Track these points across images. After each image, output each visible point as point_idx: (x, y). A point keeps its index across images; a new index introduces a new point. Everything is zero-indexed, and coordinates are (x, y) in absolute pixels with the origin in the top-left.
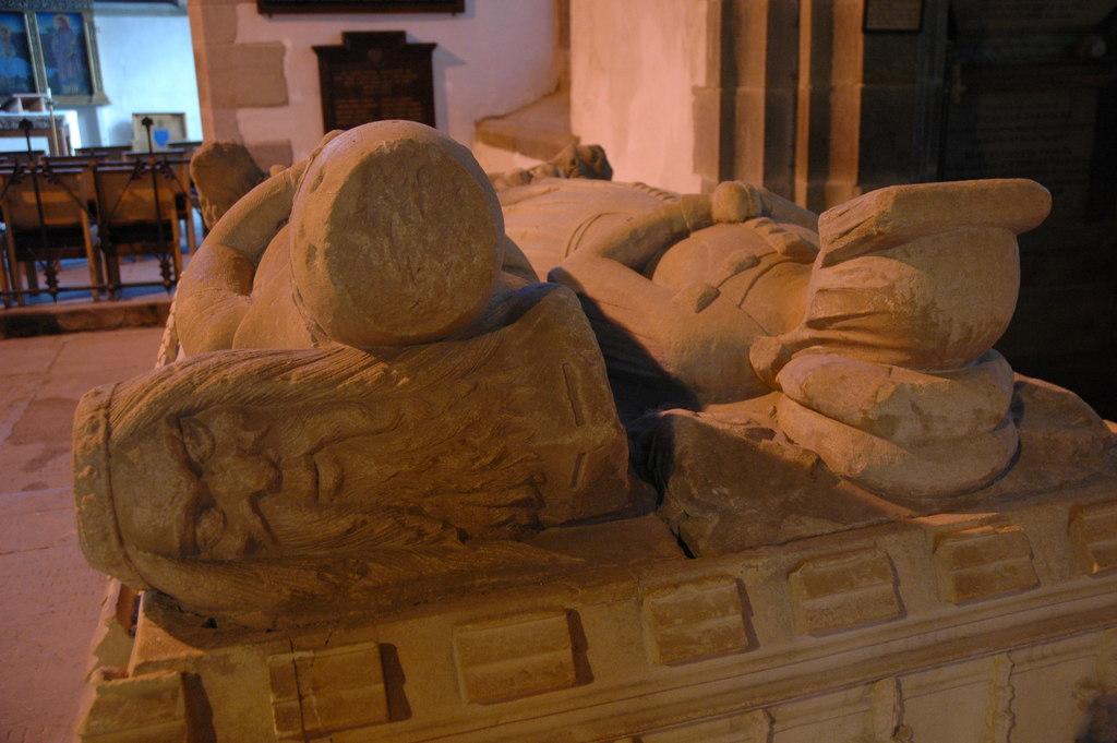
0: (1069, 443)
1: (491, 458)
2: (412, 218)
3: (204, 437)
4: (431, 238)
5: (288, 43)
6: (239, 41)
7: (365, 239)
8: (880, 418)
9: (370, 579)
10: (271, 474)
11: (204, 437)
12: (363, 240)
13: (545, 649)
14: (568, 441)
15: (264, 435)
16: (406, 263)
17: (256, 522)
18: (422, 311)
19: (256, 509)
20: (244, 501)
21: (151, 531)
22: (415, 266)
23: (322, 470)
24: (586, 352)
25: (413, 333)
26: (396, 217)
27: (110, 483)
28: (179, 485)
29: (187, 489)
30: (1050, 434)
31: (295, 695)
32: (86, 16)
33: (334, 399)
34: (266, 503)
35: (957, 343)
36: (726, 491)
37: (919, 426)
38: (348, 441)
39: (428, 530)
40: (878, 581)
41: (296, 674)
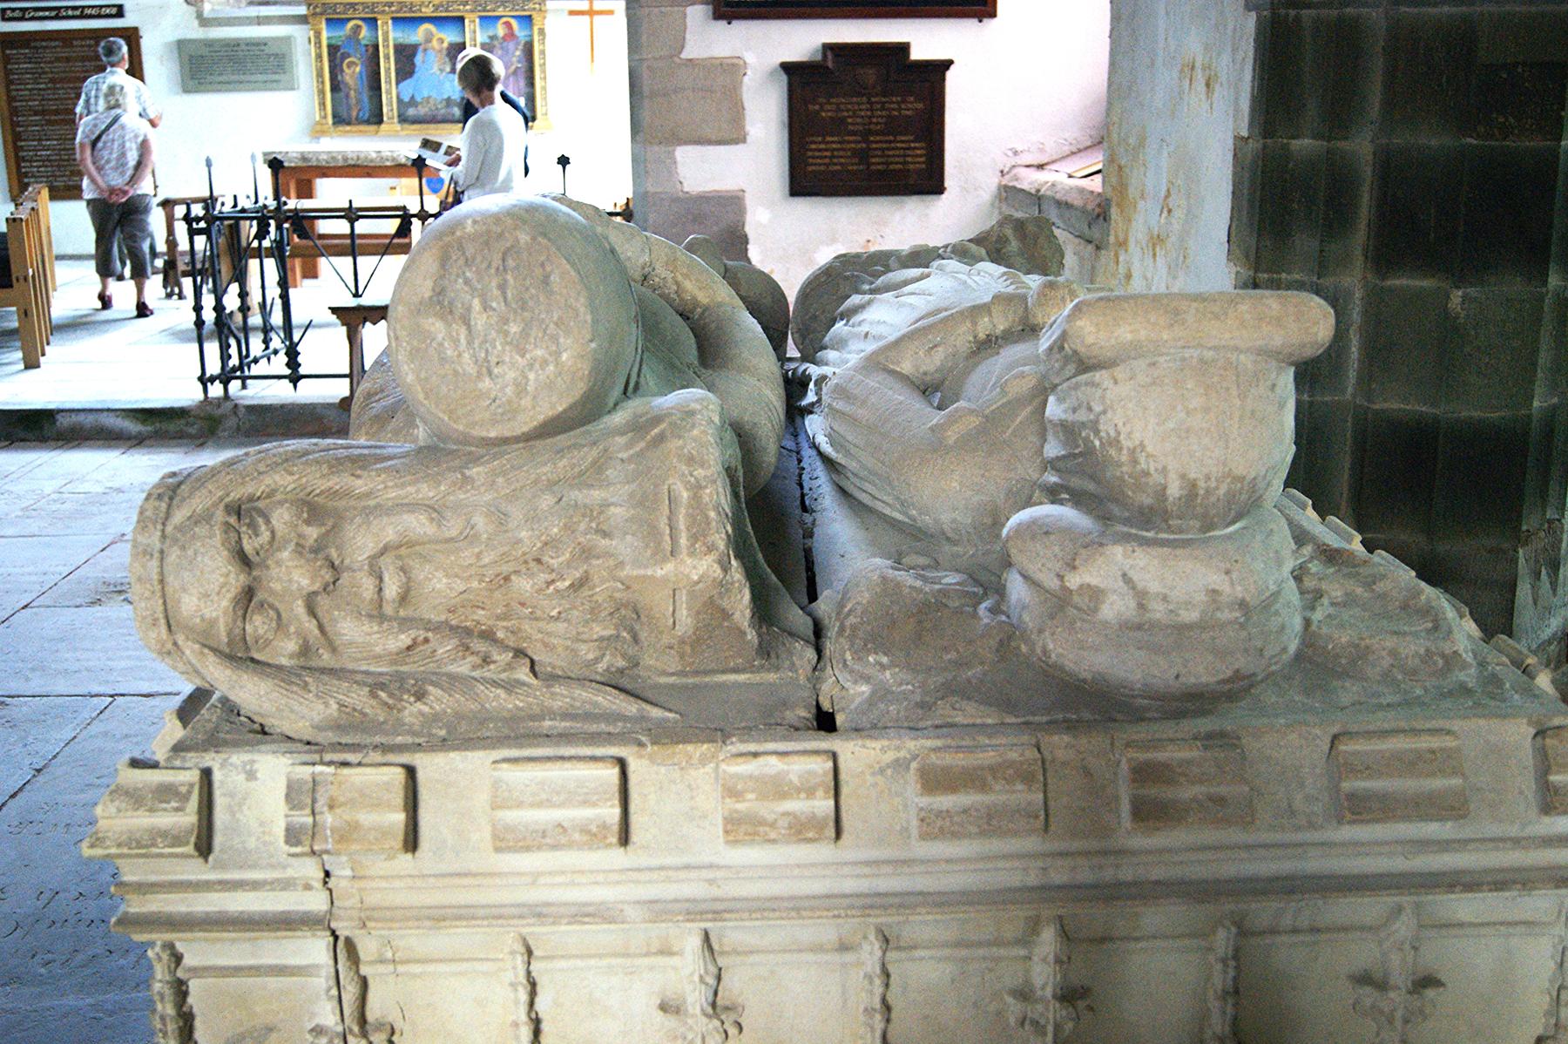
0: (1384, 653)
1: (567, 583)
2: (494, 305)
3: (263, 528)
4: (514, 328)
5: (750, 58)
6: (684, 56)
7: (439, 325)
8: (1081, 586)
9: (425, 704)
10: (328, 576)
11: (263, 528)
12: (437, 327)
13: (585, 803)
14: (659, 573)
15: (328, 532)
16: (483, 355)
17: (311, 626)
18: (500, 410)
19: (312, 612)
20: (300, 602)
21: (198, 620)
22: (493, 360)
23: (386, 578)
24: (699, 473)
25: (493, 434)
26: (476, 303)
27: (162, 567)
28: (228, 575)
29: (237, 580)
30: (1362, 639)
31: (308, 811)
32: (537, 18)
33: (406, 501)
34: (323, 602)
35: (1180, 499)
36: (885, 660)
37: (1132, 604)
38: (417, 548)
39: (496, 657)
40: (1019, 787)
41: (314, 790)
